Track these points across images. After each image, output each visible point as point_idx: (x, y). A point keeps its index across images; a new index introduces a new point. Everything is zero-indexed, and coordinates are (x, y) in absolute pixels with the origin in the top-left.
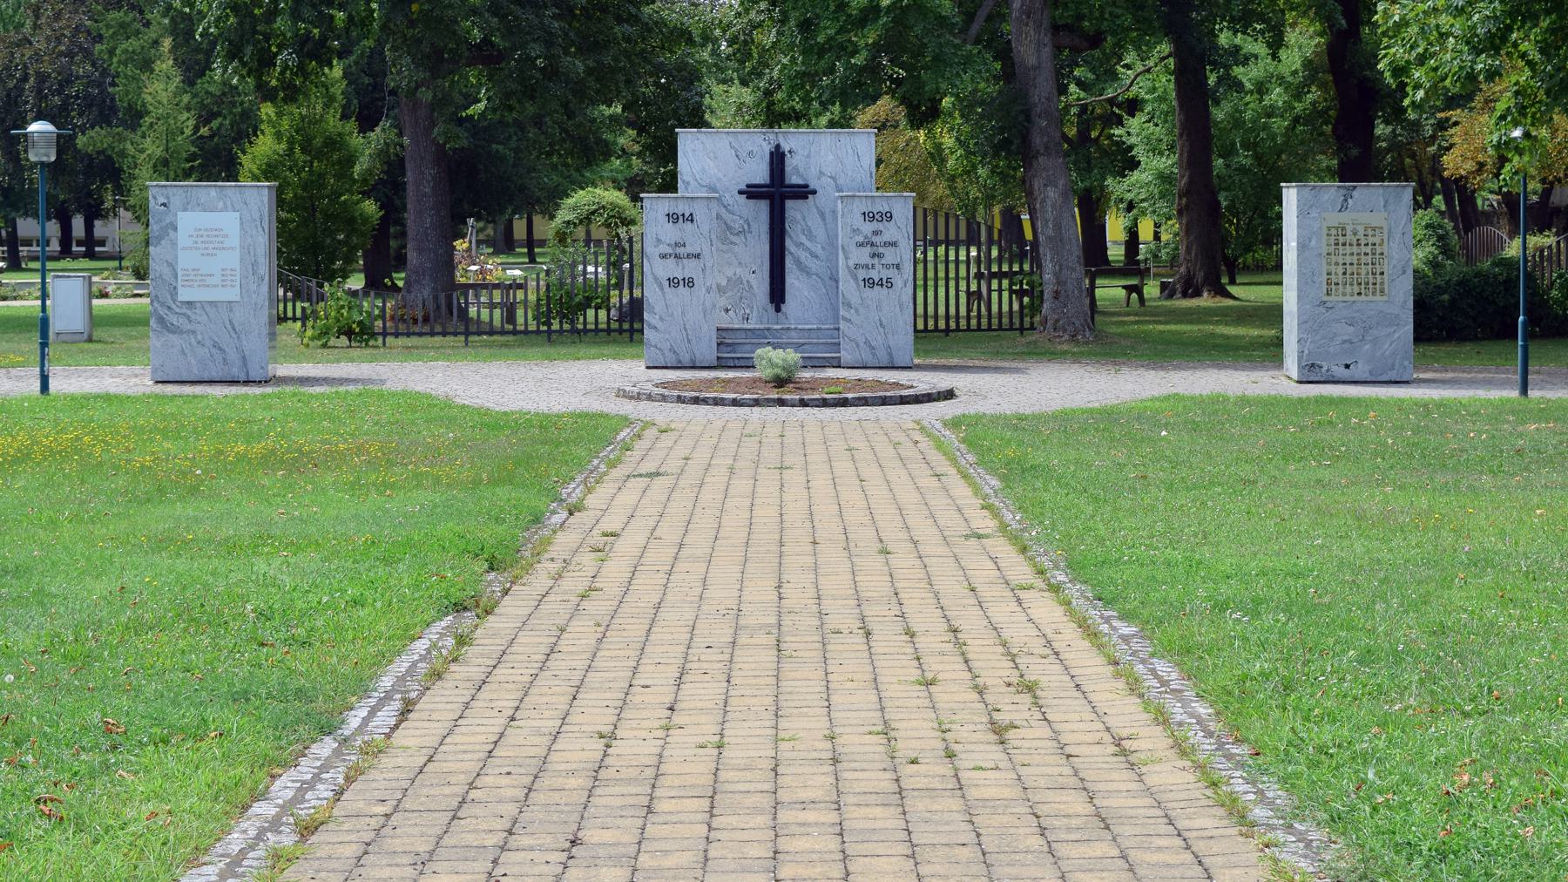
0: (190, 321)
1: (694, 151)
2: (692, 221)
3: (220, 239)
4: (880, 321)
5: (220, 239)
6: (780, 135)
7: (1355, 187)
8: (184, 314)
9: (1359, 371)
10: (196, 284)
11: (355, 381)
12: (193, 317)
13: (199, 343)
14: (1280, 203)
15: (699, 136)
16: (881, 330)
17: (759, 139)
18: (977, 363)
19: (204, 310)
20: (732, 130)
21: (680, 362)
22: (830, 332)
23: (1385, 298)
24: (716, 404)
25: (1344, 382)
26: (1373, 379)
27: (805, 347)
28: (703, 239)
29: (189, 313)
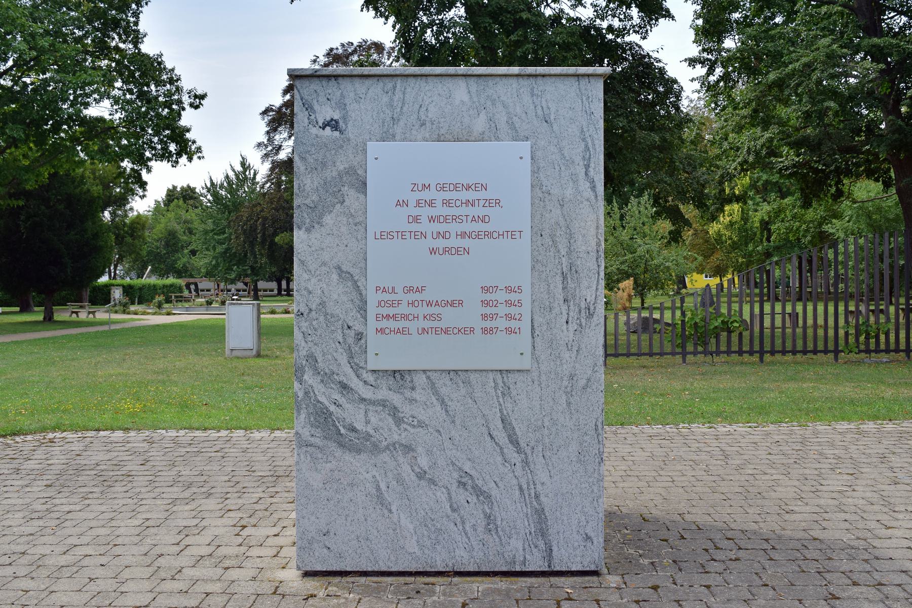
0: (399, 421)
5: (478, 211)
10: (413, 326)
19: (436, 393)
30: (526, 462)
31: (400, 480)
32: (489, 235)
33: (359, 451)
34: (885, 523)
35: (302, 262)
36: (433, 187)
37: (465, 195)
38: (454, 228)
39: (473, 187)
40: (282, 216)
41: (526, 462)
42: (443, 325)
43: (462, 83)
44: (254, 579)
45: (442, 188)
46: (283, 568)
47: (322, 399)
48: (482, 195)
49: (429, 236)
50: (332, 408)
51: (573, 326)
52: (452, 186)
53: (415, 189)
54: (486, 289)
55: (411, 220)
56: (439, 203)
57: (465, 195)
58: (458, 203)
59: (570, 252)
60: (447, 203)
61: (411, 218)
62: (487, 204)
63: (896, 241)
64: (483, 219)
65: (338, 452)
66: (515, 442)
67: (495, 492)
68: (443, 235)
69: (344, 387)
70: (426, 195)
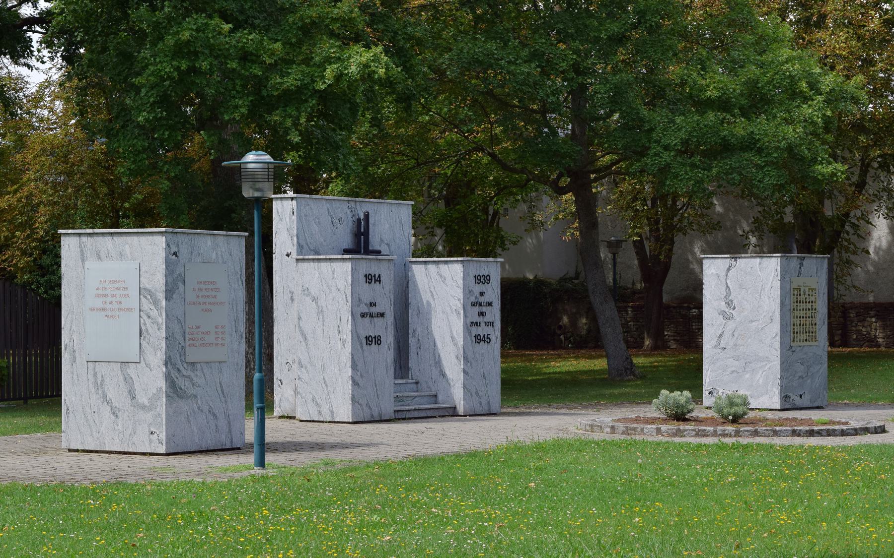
0: (193, 384)
1: (306, 216)
2: (380, 281)
3: (214, 293)
4: (324, 379)
5: (214, 293)
6: (358, 203)
7: (804, 257)
8: (189, 377)
9: (805, 402)
10: (198, 343)
11: (319, 447)
12: (195, 379)
13: (199, 408)
14: (60, 289)
15: (311, 202)
16: (484, 380)
17: (345, 206)
18: (510, 410)
19: (203, 372)
20: (331, 197)
21: (380, 415)
22: (412, 386)
23: (816, 343)
24: (829, 435)
25: (801, 409)
26: (811, 405)
27: (417, 399)
28: (386, 299)
29: (192, 375)
30: (226, 402)
31: (193, 411)
32: (217, 303)
33: (183, 398)
35: (456, 344)
38: (208, 300)
40: (46, 260)
41: (226, 402)
42: (205, 342)
43: (209, 237)
44: (382, 240)
45: (110, 282)
48: (123, 285)
50: (176, 380)
51: (238, 343)
54: (216, 327)
59: (73, 373)
60: (110, 288)
63: (481, 136)
64: (215, 297)
65: (177, 399)
66: (223, 392)
67: (218, 415)
68: (114, 296)
69: (149, 317)
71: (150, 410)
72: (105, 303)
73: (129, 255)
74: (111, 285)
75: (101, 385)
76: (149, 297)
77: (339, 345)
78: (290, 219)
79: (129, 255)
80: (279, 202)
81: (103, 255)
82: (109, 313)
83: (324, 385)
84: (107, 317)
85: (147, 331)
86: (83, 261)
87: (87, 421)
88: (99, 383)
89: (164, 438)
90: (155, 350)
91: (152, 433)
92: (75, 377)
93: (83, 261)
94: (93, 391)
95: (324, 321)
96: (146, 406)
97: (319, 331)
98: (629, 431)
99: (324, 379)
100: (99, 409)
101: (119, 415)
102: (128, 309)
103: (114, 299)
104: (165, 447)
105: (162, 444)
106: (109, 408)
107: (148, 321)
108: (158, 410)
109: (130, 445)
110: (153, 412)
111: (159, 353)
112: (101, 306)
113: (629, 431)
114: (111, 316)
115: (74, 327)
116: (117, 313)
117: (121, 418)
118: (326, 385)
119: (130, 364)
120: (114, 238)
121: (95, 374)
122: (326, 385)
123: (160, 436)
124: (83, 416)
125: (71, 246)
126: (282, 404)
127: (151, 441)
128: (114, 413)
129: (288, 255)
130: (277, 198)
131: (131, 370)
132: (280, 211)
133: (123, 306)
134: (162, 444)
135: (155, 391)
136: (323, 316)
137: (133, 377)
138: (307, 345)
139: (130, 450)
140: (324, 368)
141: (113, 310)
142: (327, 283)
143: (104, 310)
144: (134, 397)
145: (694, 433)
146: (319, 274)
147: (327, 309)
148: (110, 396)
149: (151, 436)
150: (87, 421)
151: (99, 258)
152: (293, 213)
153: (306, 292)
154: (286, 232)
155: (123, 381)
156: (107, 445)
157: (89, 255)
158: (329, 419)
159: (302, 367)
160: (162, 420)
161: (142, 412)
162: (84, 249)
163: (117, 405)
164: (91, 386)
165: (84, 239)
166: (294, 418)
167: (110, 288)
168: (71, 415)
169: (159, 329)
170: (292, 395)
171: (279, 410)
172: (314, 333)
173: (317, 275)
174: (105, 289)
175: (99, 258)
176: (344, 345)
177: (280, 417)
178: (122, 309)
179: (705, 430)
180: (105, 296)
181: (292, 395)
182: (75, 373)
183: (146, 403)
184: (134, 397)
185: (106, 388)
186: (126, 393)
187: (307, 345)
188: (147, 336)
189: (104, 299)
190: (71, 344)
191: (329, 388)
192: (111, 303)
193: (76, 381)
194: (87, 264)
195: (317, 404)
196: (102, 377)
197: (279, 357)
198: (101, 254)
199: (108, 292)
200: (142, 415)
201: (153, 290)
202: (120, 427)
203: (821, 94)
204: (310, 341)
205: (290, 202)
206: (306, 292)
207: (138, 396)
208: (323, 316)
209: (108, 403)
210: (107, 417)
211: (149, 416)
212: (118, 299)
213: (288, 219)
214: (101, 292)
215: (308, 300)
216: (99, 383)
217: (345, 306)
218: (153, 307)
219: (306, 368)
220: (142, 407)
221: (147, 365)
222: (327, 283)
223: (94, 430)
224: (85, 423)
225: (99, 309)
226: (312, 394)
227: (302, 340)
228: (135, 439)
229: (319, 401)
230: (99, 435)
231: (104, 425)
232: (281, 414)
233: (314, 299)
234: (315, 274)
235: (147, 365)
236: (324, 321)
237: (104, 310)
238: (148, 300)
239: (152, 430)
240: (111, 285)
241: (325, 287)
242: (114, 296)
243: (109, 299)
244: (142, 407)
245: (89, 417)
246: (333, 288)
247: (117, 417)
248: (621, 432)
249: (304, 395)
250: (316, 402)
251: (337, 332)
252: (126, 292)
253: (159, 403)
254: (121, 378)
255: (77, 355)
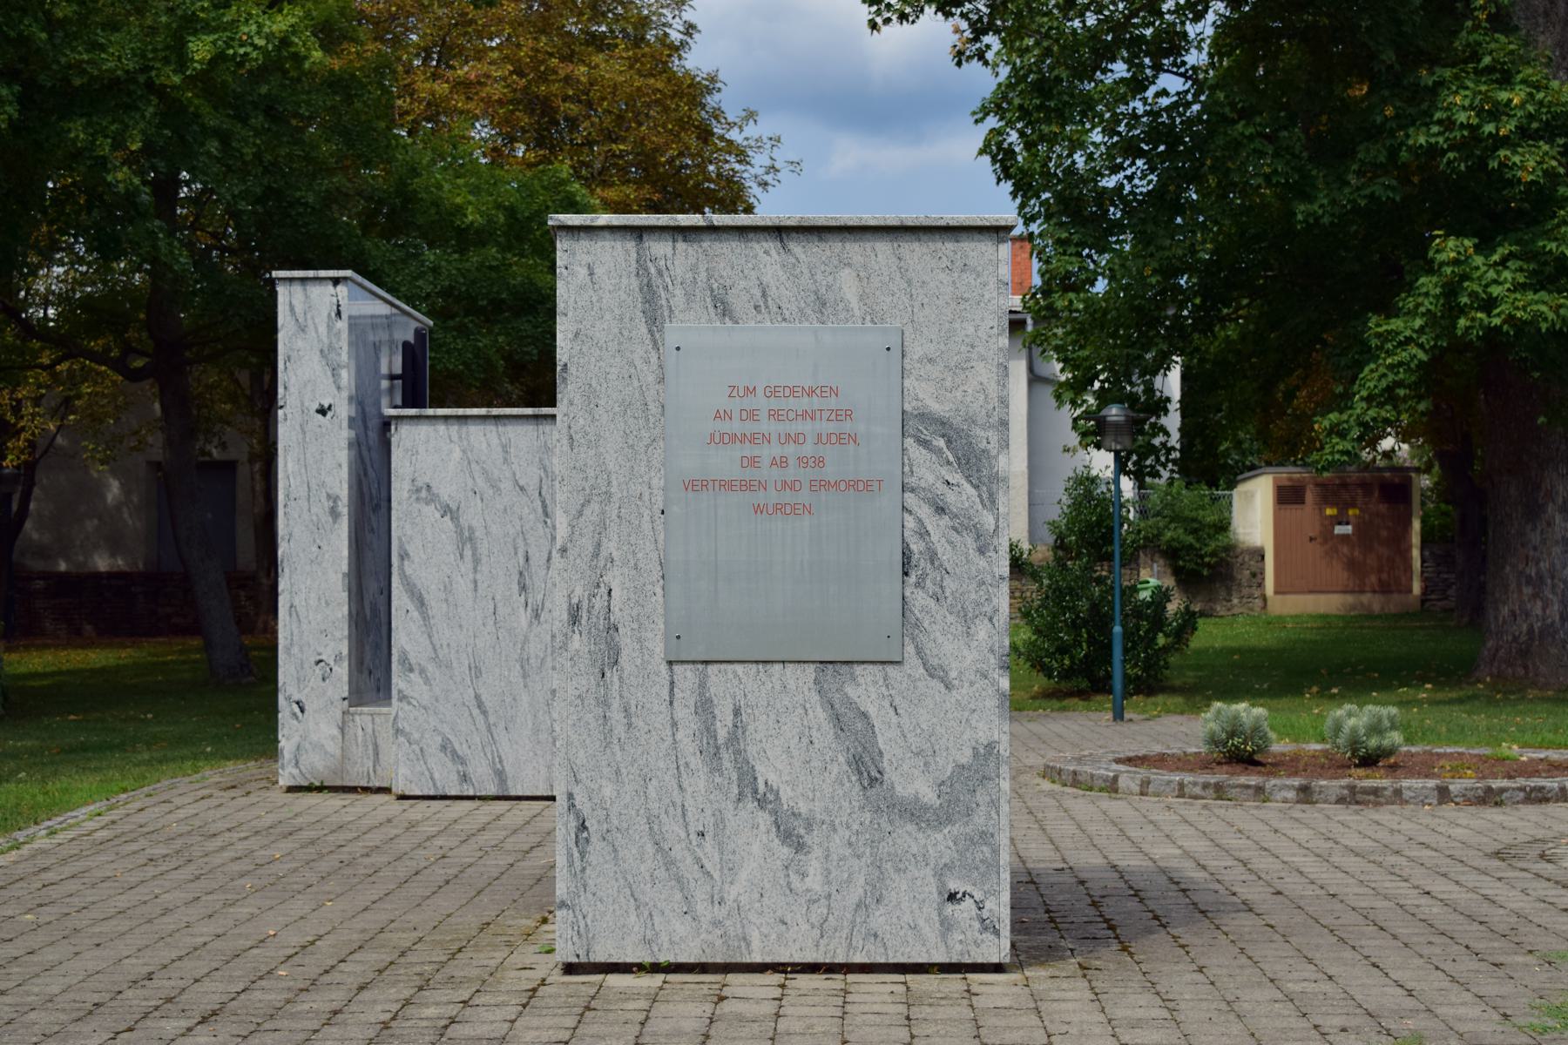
4: (477, 697)
34: (1489, 879)
36: (760, 391)
37: (804, 403)
39: (818, 391)
45: (772, 392)
46: (151, 860)
47: (969, 490)
48: (833, 403)
49: (774, 439)
52: (787, 390)
53: (735, 393)
55: (744, 417)
56: (763, 415)
57: (804, 403)
58: (792, 416)
59: (605, 703)
60: (774, 415)
61: (744, 413)
62: (833, 417)
68: (796, 439)
69: (941, 510)
70: (749, 403)
71: (942, 818)
72: (753, 462)
73: (854, 303)
74: (774, 404)
75: (733, 739)
76: (941, 443)
77: (524, 618)
78: (330, 328)
79: (854, 303)
80: (297, 288)
81: (738, 302)
82: (772, 497)
83: (476, 712)
84: (758, 509)
85: (933, 556)
86: (654, 321)
87: (669, 864)
88: (722, 734)
89: (1005, 914)
90: (967, 619)
91: (952, 897)
92: (616, 715)
93: (654, 321)
94: (696, 762)
95: (476, 561)
96: (926, 808)
97: (462, 586)
98: (1359, 797)
99: (477, 697)
100: (720, 823)
101: (808, 839)
102: (852, 485)
103: (790, 450)
104: (1006, 944)
105: (997, 933)
106: (764, 819)
107: (937, 527)
108: (979, 819)
109: (858, 941)
110: (957, 829)
111: (982, 631)
112: (734, 472)
113: (1359, 797)
114: (779, 508)
115: (611, 547)
116: (804, 496)
117: (817, 852)
118: (484, 713)
119: (858, 669)
120: (792, 245)
121: (705, 707)
122: (484, 713)
123: (988, 905)
124: (650, 849)
125: (599, 271)
126: (303, 759)
127: (947, 926)
128: (787, 836)
129: (322, 411)
130: (291, 280)
131: (865, 689)
132: (299, 309)
133: (830, 472)
134: (997, 933)
135: (965, 757)
136: (474, 550)
137: (872, 710)
138: (425, 617)
139: (859, 958)
140: (476, 671)
141: (790, 486)
142: (485, 472)
143: (747, 486)
144: (873, 781)
145: (1522, 795)
146: (464, 452)
147: (488, 533)
148: (773, 779)
149: (950, 908)
150: (669, 864)
151: (724, 310)
152: (339, 314)
153: (424, 494)
154: (317, 357)
155: (828, 728)
156: (756, 944)
157: (679, 299)
158: (492, 790)
159: (411, 670)
160: (996, 851)
161: (910, 827)
162: (656, 281)
163: (803, 808)
164: (688, 746)
165: (659, 248)
166: (386, 790)
167: (774, 415)
168: (596, 845)
169: (982, 551)
170: (333, 738)
171: (295, 772)
172: (447, 588)
173: (457, 454)
174: (752, 415)
175: (724, 310)
176: (537, 616)
177: (291, 789)
178: (825, 485)
179: (1543, 788)
180: (753, 439)
181: (333, 738)
182: (616, 704)
183: (929, 796)
184: (873, 781)
185: (752, 750)
186: (840, 765)
187: (425, 617)
188: (933, 574)
189: (748, 450)
190: (599, 603)
191: (492, 719)
192: (782, 462)
193: (620, 730)
194: (673, 333)
195: (457, 757)
196: (737, 712)
197: (295, 650)
198: (730, 299)
199: (766, 426)
200: (908, 838)
201: (957, 421)
202: (814, 882)
203: (1264, 174)
204: (436, 607)
205: (330, 288)
206: (424, 494)
207: (891, 775)
208: (474, 550)
209: (762, 803)
210: (756, 848)
211: (940, 843)
212: (808, 449)
213: (323, 329)
214: (736, 426)
215: (431, 512)
216: (722, 734)
217: (540, 526)
218: (956, 478)
219: (422, 671)
220: (913, 812)
221: (934, 672)
222: (485, 472)
223: (700, 894)
224: (661, 873)
225: (728, 485)
226: (440, 733)
227: (411, 607)
228: (878, 920)
229: (462, 750)
230: (720, 912)
231: (743, 875)
232: (292, 783)
233: (446, 511)
234: (451, 452)
235: (934, 672)
236: (476, 561)
237: (747, 486)
238: (939, 452)
239: (953, 885)
240: (774, 404)
241: (481, 482)
242: (796, 439)
243: (766, 452)
244: (913, 812)
245: (678, 852)
246: (506, 485)
247: (800, 847)
248: (1333, 798)
249: (416, 736)
250: (454, 752)
251: (515, 587)
252: (847, 426)
253: (981, 797)
254: (820, 715)
255: (625, 639)
